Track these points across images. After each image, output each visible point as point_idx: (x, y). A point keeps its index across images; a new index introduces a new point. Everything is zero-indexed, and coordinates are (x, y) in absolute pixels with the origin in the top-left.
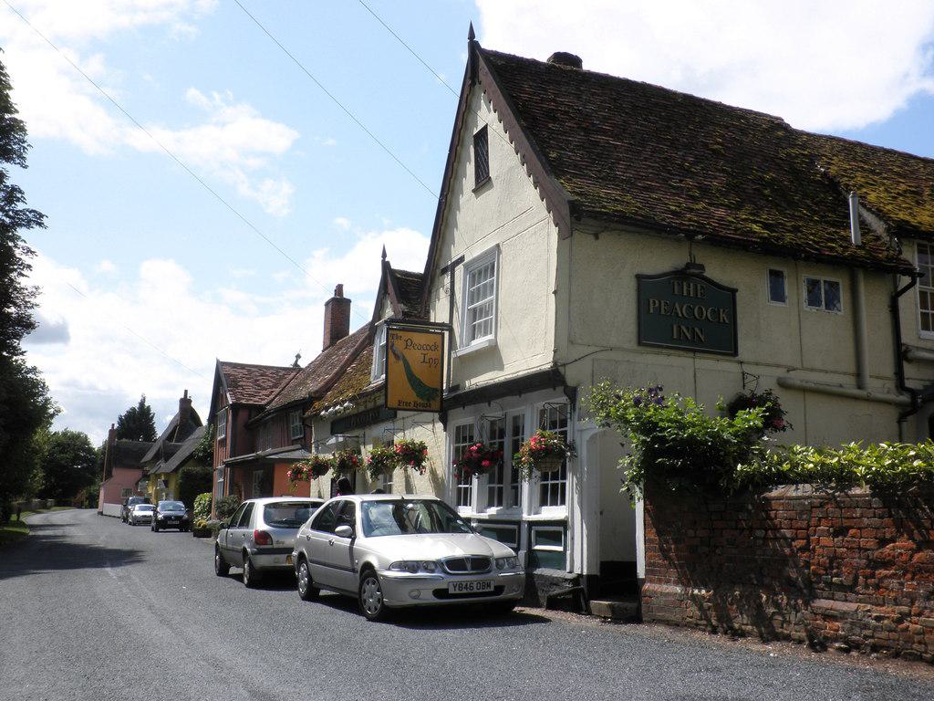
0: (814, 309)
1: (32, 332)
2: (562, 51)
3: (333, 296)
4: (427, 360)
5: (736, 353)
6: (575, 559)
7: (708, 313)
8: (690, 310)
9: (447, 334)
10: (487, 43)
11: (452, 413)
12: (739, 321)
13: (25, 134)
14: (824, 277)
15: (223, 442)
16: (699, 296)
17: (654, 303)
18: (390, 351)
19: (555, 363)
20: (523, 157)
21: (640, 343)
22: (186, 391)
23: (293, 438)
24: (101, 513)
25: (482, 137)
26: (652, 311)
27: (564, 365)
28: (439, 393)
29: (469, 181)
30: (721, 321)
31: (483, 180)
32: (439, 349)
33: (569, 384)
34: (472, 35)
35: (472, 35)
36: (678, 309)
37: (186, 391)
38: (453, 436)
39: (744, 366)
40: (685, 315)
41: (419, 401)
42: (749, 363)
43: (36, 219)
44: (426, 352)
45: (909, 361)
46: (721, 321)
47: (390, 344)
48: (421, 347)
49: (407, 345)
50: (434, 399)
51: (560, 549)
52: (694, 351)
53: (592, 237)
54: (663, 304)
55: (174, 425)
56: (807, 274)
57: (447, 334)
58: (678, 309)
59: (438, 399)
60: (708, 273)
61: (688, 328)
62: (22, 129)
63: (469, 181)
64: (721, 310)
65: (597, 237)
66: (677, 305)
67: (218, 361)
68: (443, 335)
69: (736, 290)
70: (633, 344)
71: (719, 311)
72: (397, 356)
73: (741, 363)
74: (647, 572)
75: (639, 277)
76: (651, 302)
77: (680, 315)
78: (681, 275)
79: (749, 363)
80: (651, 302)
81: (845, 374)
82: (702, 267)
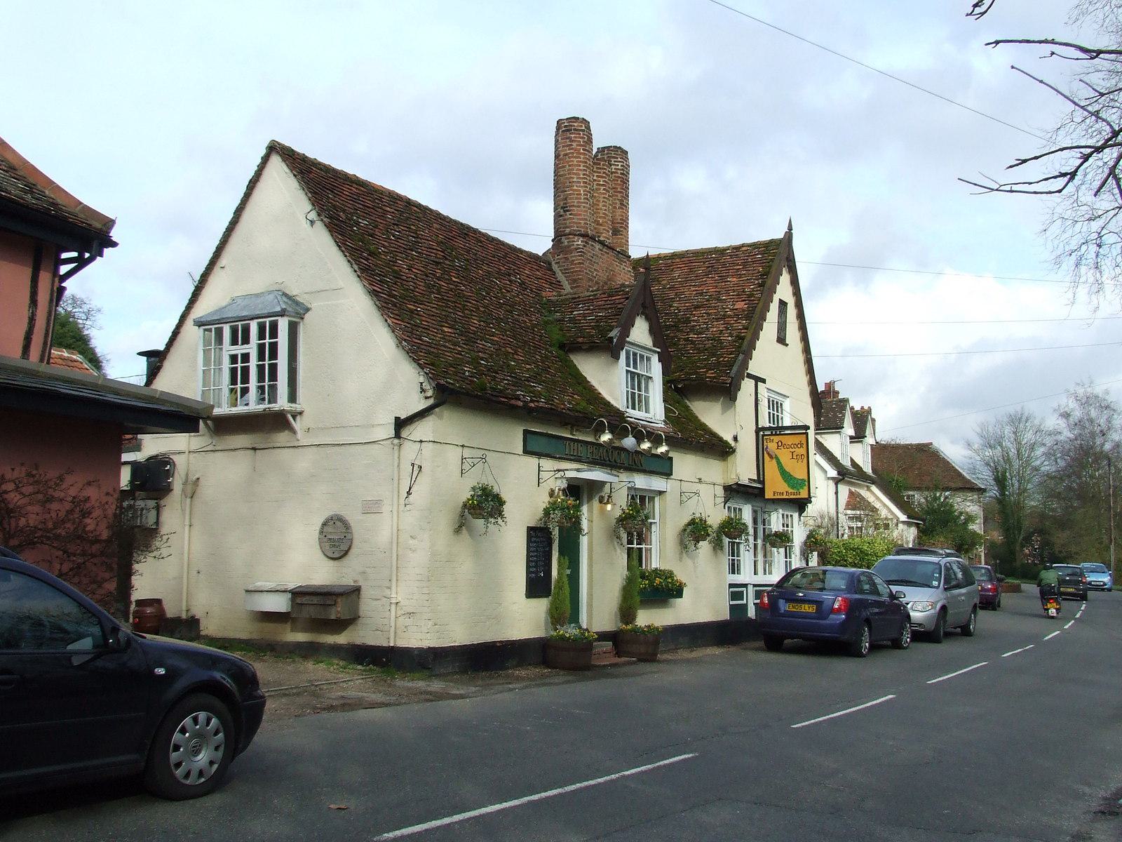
44: (792, 450)
72: (771, 457)
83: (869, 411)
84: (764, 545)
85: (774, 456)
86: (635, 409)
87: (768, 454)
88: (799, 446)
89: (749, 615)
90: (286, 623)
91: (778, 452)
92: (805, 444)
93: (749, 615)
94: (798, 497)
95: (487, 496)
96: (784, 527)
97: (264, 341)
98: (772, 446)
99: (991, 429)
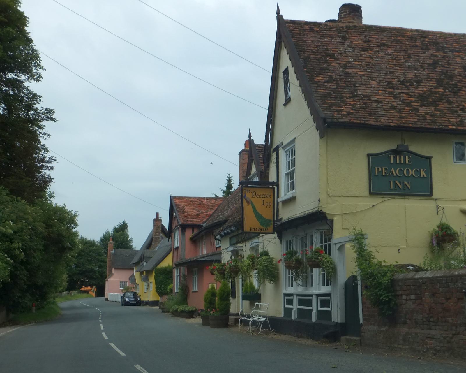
1: (53, 171)
2: (347, 3)
3: (244, 148)
4: (265, 204)
5: (431, 195)
7: (413, 172)
9: (276, 187)
10: (287, 16)
16: (407, 162)
17: (378, 169)
18: (244, 199)
20: (302, 90)
22: (157, 214)
23: (216, 246)
24: (107, 300)
25: (286, 72)
26: (377, 174)
28: (272, 223)
30: (422, 176)
31: (288, 101)
32: (272, 196)
34: (278, 12)
35: (278, 12)
37: (157, 214)
38: (285, 246)
39: (437, 201)
40: (398, 175)
41: (262, 227)
43: (49, 114)
46: (422, 176)
47: (244, 195)
49: (253, 195)
51: (329, 309)
54: (384, 169)
55: (151, 237)
57: (276, 187)
61: (400, 182)
64: (422, 170)
66: (393, 169)
68: (274, 188)
69: (432, 157)
70: (366, 193)
71: (420, 170)
72: (248, 202)
73: (436, 200)
74: (364, 320)
75: (369, 155)
76: (376, 168)
77: (395, 175)
78: (396, 152)
80: (376, 168)
82: (407, 146)
88: (268, 196)
91: (253, 200)
98: (249, 195)
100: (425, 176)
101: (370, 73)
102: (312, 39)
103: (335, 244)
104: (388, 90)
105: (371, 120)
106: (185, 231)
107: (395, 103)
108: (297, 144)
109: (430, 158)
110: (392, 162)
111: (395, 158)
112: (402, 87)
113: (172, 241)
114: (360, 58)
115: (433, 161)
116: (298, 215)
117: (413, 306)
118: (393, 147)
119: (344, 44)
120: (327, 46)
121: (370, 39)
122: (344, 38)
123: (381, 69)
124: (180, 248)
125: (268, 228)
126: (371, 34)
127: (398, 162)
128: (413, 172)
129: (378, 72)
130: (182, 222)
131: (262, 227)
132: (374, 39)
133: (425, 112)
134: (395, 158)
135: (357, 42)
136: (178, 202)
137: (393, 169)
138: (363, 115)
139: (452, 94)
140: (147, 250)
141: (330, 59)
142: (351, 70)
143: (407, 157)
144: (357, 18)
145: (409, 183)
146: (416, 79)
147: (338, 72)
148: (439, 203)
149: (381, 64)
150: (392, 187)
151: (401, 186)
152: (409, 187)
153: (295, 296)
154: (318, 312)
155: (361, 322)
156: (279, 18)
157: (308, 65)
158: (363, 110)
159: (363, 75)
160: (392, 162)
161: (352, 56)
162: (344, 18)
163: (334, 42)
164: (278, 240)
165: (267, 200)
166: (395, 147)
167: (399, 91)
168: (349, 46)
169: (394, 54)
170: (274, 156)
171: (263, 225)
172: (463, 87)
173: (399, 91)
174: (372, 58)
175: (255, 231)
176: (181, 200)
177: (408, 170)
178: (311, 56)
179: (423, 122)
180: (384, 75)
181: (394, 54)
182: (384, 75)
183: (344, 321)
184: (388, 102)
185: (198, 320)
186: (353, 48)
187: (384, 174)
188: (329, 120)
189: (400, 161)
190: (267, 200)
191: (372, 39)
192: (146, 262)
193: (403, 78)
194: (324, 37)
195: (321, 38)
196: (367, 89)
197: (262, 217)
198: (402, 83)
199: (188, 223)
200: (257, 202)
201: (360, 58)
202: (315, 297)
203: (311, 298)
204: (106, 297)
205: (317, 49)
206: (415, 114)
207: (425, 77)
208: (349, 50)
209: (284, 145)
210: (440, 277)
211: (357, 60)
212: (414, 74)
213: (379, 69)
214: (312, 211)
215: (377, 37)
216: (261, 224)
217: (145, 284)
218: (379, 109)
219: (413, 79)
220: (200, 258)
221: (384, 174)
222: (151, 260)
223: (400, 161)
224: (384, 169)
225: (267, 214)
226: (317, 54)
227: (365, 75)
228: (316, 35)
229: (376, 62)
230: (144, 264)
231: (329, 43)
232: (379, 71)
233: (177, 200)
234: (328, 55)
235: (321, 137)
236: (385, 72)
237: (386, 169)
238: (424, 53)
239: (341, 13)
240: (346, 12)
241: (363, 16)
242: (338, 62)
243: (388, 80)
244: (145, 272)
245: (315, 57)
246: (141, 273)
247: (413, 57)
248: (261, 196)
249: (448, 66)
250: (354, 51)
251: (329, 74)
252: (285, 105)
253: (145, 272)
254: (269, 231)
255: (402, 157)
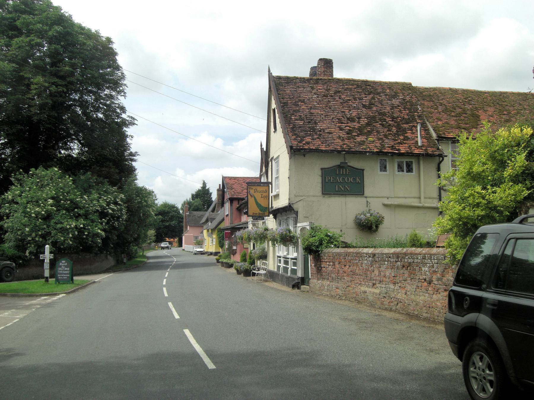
0: (401, 173)
2: (322, 58)
4: (263, 197)
5: (363, 194)
6: (272, 261)
7: (351, 180)
8: (343, 179)
9: (270, 185)
10: (275, 74)
11: (279, 215)
12: (365, 180)
13: (121, 92)
14: (405, 160)
15: (227, 215)
16: (347, 173)
18: (249, 194)
19: (289, 203)
21: (323, 194)
25: (274, 110)
27: (293, 204)
28: (268, 209)
29: (272, 129)
30: (357, 182)
32: (268, 192)
33: (295, 210)
34: (269, 71)
35: (269, 71)
36: (338, 179)
39: (368, 199)
41: (261, 212)
42: (370, 197)
44: (262, 194)
45: (445, 190)
46: (357, 182)
47: (248, 191)
48: (260, 192)
50: (266, 211)
52: (346, 195)
53: (303, 156)
54: (332, 178)
56: (397, 160)
58: (338, 179)
59: (268, 211)
60: (349, 164)
62: (153, 192)
63: (272, 129)
64: (357, 178)
65: (304, 156)
67: (271, 77)
68: (269, 186)
69: (364, 170)
70: (320, 194)
72: (251, 196)
73: (366, 197)
74: (311, 276)
75: (322, 169)
76: (327, 177)
78: (340, 167)
79: (370, 197)
80: (327, 177)
81: (414, 198)
83: (416, 235)
84: (305, 255)
85: (253, 196)
86: (403, 171)
87: (250, 195)
88: (265, 192)
89: (171, 303)
90: (165, 205)
91: (255, 194)
92: (268, 191)
93: (171, 303)
94: (461, 261)
95: (39, 214)
96: (230, 266)
97: (405, 170)
98: (252, 191)
99: (188, 200)
100: (360, 182)
101: (327, 113)
102: (290, 89)
103: (299, 227)
104: (337, 124)
105: (323, 146)
106: (233, 203)
107: (342, 134)
108: (280, 158)
109: (363, 170)
110: (337, 173)
111: (340, 171)
112: (347, 122)
113: (224, 210)
114: (322, 102)
115: (365, 172)
116: (280, 206)
117: (331, 269)
118: (338, 163)
119: (312, 92)
120: (300, 94)
121: (330, 88)
122: (312, 88)
123: (335, 110)
124: (229, 215)
125: (265, 213)
126: (331, 84)
127: (341, 173)
128: (351, 180)
129: (333, 112)
130: (230, 196)
131: (261, 212)
132: (333, 88)
133: (360, 139)
134: (340, 171)
135: (322, 91)
136: (228, 181)
137: (338, 178)
138: (317, 143)
139: (381, 126)
140: (212, 213)
141: (301, 104)
142: (314, 111)
143: (347, 170)
144: (329, 68)
145: (348, 186)
146: (358, 116)
147: (305, 113)
148: (369, 200)
149: (336, 106)
150: (337, 190)
151: (343, 189)
152: (349, 189)
153: (282, 258)
154: (292, 269)
155: (310, 277)
156: (270, 74)
157: (286, 108)
158: (318, 139)
159: (322, 114)
160: (337, 173)
161: (316, 101)
162: (320, 68)
163: (305, 91)
164: (275, 220)
165: (265, 194)
166: (339, 164)
167: (346, 125)
168: (315, 94)
169: (345, 98)
170: (270, 163)
171: (262, 211)
172: (390, 121)
173: (346, 125)
174: (330, 102)
175: (256, 215)
176: (230, 179)
177: (348, 179)
178: (289, 102)
179: (357, 147)
180: (336, 113)
181: (345, 98)
182: (336, 113)
183: (303, 276)
184: (337, 133)
185: (233, 270)
186: (318, 95)
187: (332, 181)
188: (294, 148)
189: (343, 172)
190: (265, 194)
191: (332, 88)
192: (211, 222)
193: (350, 116)
194: (299, 87)
195: (297, 88)
196: (324, 124)
197: (261, 205)
198: (348, 119)
199: (235, 197)
200: (258, 196)
201: (322, 102)
202: (290, 259)
203: (288, 260)
204: (183, 248)
205: (292, 96)
206: (353, 141)
207: (364, 114)
208: (315, 96)
209: (275, 158)
210: (343, 252)
211: (320, 104)
212: (357, 113)
213: (334, 110)
214: (285, 205)
215: (335, 86)
216: (260, 210)
217: (210, 239)
218: (329, 138)
219: (356, 116)
220: (237, 226)
221: (332, 181)
222: (214, 221)
223: (343, 172)
224: (332, 178)
225: (263, 204)
226: (293, 100)
227: (324, 114)
228: (294, 86)
229: (333, 104)
230: (210, 223)
231: (302, 92)
232: (334, 111)
233: (227, 180)
234: (300, 101)
235: (290, 158)
236: (337, 112)
237: (333, 178)
238: (366, 97)
239: (319, 65)
240: (322, 64)
241: (333, 66)
242: (307, 105)
243: (339, 117)
244: (210, 230)
245: (291, 103)
246: (208, 231)
247: (358, 100)
248: (260, 192)
249: (381, 106)
250: (318, 97)
251: (299, 114)
252: (275, 132)
253: (210, 230)
254: (266, 215)
255: (344, 170)
